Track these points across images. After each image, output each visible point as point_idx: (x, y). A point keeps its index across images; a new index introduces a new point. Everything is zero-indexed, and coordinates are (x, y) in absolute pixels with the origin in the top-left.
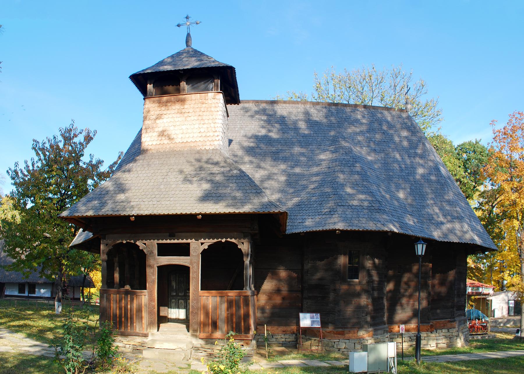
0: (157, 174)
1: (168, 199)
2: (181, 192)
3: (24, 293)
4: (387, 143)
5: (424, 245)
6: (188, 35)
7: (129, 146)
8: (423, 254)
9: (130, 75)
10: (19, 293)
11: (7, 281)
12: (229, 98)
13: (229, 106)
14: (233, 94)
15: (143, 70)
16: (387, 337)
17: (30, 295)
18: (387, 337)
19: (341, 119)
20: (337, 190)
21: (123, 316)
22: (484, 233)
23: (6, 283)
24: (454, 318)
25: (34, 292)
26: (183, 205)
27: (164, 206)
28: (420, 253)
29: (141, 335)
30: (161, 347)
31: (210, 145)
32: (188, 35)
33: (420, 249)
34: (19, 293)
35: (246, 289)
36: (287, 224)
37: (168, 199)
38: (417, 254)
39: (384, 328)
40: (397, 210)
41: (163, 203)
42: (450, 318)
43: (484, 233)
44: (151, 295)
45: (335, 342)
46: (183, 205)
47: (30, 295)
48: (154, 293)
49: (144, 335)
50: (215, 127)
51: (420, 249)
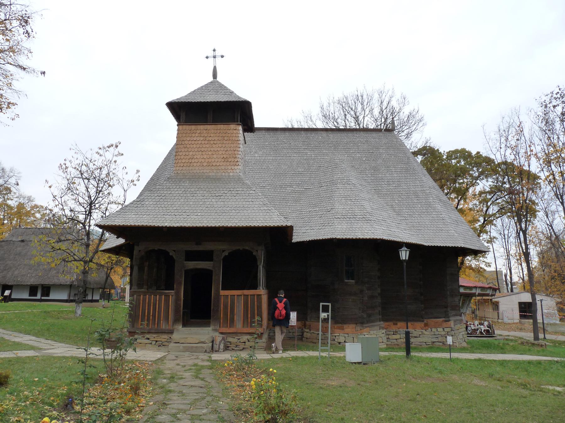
0: (187, 192)
1: (196, 214)
2: (207, 209)
3: (36, 296)
4: (376, 161)
5: (407, 251)
6: (215, 68)
7: (161, 163)
8: (407, 259)
9: (166, 102)
10: (30, 296)
11: (15, 283)
12: (246, 127)
13: (246, 134)
14: (250, 125)
15: (177, 99)
16: (383, 333)
17: (43, 298)
18: (383, 333)
19: (336, 143)
20: (334, 205)
21: (151, 314)
22: (473, 236)
23: (15, 285)
24: (449, 317)
25: (48, 295)
26: (209, 219)
27: (193, 219)
28: (404, 258)
29: (167, 332)
30: (185, 341)
31: (231, 169)
32: (215, 68)
33: (404, 254)
34: (30, 296)
35: (260, 289)
36: (294, 234)
37: (196, 214)
38: (401, 259)
39: (380, 325)
40: (386, 220)
41: (192, 217)
42: (445, 318)
43: (473, 236)
44: (177, 294)
45: (335, 336)
46: (209, 219)
47: (43, 298)
48: (181, 293)
49: (170, 332)
50: (235, 154)
51: (404, 254)
